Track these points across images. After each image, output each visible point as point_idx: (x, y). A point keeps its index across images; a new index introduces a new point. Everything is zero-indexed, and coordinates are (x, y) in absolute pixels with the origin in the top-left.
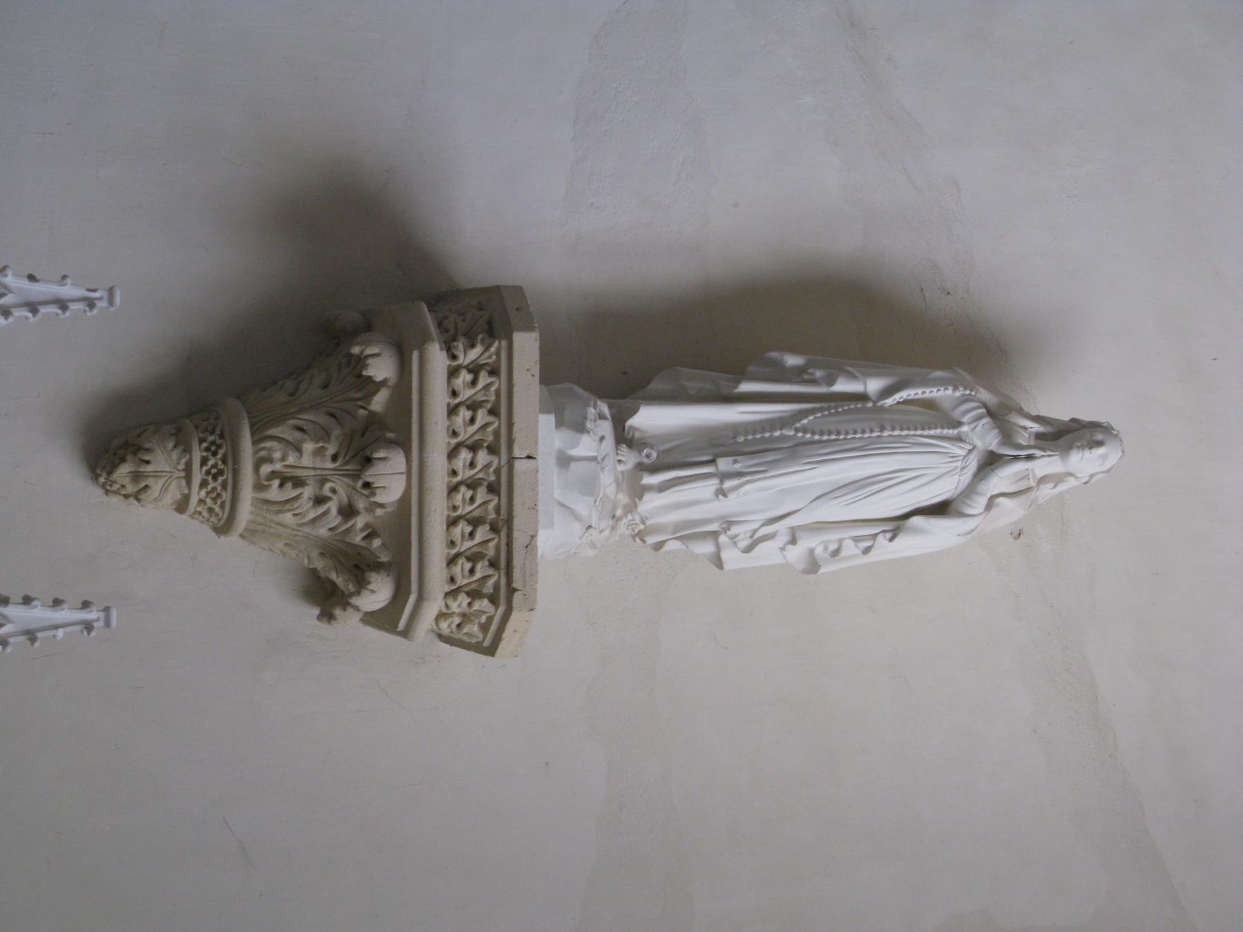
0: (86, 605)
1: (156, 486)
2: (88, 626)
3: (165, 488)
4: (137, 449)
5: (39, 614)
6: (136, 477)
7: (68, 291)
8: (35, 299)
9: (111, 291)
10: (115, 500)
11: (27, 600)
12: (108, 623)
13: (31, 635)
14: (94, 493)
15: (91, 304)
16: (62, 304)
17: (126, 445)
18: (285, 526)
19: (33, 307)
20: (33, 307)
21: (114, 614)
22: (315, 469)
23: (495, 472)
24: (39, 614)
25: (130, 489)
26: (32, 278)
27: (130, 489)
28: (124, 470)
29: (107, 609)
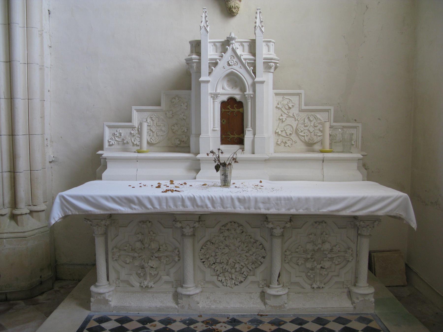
0: (256, 13)
1: (237, 5)
2: (260, 12)
3: (237, 3)
4: (230, 8)
5: (258, 21)
6: (235, 8)
7: (204, 16)
8: (205, 21)
9: (203, 9)
10: (239, 12)
11: (256, 23)
12: (260, 9)
13: (261, 22)
14: (238, 15)
15: (206, 12)
16: (206, 17)
17: (230, 10)
18: (304, 279)
19: (206, 21)
20: (206, 21)
21: (258, 8)
22: (42, 93)
23: (320, 264)
24: (258, 21)
25: (237, 9)
26: (202, 22)
27: (237, 9)
28: (234, 10)
29: (257, 9)
